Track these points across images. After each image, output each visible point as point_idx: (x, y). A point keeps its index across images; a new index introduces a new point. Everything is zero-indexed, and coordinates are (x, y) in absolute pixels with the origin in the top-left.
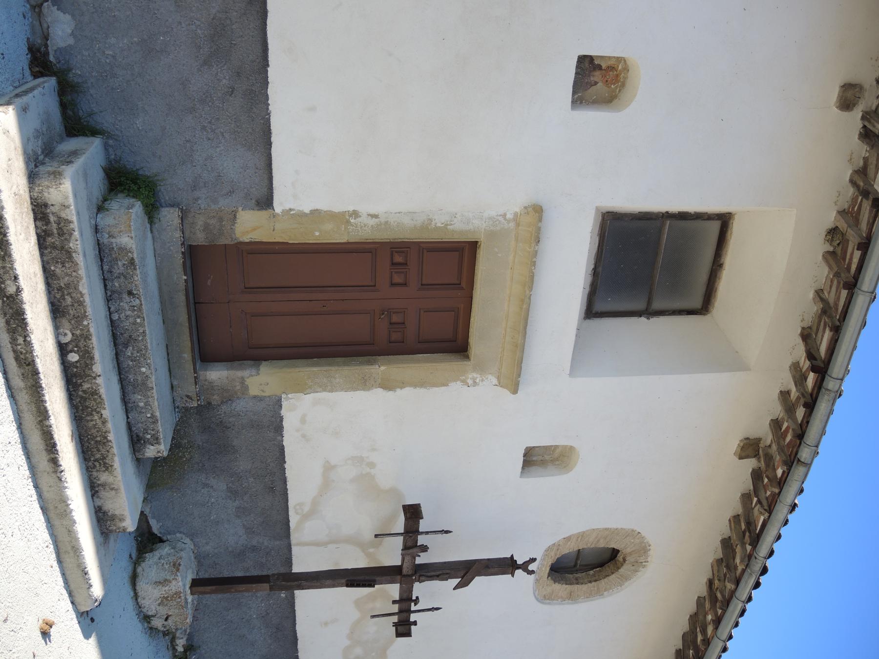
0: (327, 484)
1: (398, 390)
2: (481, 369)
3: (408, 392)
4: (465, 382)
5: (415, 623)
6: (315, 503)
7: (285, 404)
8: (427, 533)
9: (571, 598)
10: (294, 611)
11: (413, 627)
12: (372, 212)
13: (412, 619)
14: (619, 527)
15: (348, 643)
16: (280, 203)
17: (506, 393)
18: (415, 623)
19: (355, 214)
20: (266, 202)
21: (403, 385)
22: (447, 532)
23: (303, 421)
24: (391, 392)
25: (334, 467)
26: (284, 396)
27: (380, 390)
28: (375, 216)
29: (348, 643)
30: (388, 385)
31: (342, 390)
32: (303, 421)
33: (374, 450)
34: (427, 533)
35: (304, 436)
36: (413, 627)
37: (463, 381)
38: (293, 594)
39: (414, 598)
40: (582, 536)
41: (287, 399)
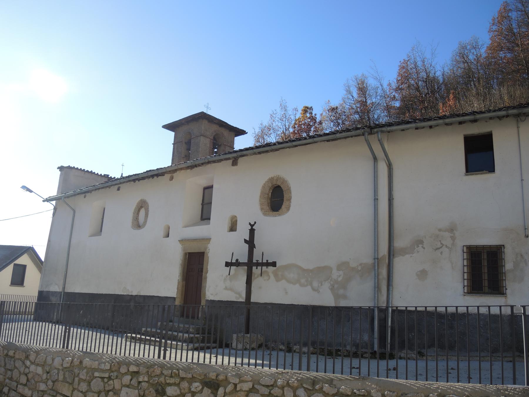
0: (231, 289)
1: (208, 269)
2: (206, 248)
3: (209, 267)
4: (208, 252)
5: (267, 261)
6: (236, 293)
7: (208, 299)
8: (232, 260)
9: (289, 200)
10: (278, 304)
11: (269, 262)
12: (178, 276)
13: (266, 262)
14: (260, 192)
15: (298, 285)
16: (175, 296)
17: (211, 240)
18: (267, 261)
19: (178, 280)
20: (174, 299)
21: (207, 268)
22: (233, 253)
23: (212, 294)
24: (208, 271)
25: (226, 287)
26: (206, 299)
27: (207, 274)
28: (179, 276)
29: (298, 285)
30: (207, 272)
31: (206, 284)
32: (212, 294)
33: (222, 276)
34: (232, 260)
35: (216, 295)
36: (269, 262)
37: (208, 253)
38: (252, 302)
39: (256, 262)
40: (262, 204)
41: (207, 298)
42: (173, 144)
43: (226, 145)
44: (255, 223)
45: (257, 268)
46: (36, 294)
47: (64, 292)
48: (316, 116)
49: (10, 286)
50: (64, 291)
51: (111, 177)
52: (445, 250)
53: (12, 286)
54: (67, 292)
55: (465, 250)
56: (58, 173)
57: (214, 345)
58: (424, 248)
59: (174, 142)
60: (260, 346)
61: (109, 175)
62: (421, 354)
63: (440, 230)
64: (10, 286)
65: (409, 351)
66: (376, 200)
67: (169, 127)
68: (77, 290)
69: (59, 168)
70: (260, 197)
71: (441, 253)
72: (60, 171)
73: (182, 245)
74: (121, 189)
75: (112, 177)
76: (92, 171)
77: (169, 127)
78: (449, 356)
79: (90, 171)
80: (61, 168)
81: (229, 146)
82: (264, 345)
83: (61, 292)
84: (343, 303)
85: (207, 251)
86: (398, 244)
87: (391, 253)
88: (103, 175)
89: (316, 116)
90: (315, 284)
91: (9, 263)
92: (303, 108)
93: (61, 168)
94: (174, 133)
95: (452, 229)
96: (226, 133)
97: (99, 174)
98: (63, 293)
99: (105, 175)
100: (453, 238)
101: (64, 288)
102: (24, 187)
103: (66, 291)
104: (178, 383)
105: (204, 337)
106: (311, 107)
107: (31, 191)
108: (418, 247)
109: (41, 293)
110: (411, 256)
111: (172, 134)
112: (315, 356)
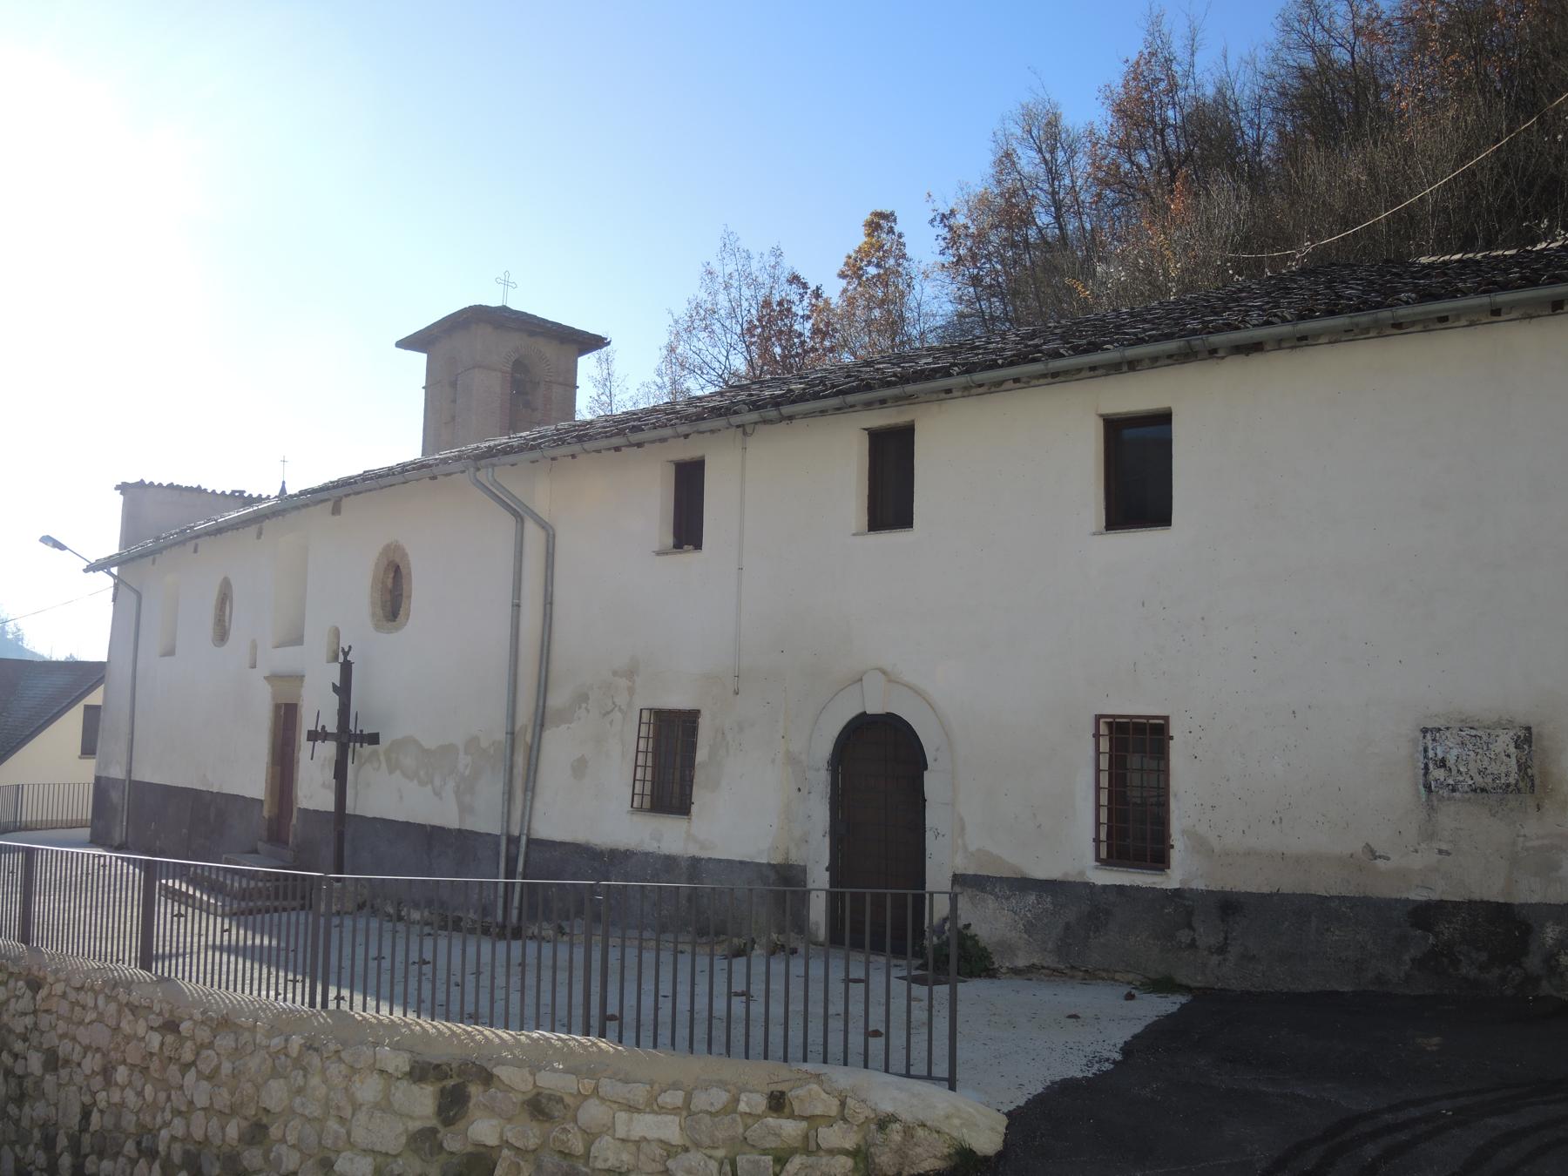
5: (361, 731)
9: (410, 597)
17: (306, 680)
18: (361, 731)
42: (423, 388)
43: (550, 382)
44: (350, 647)
45: (361, 746)
46: (92, 780)
47: (130, 780)
48: (901, 240)
49: (80, 758)
50: (130, 777)
51: (250, 495)
52: (617, 715)
53: (84, 758)
54: (137, 779)
55: (645, 717)
56: (118, 499)
57: (294, 904)
58: (588, 711)
59: (426, 382)
60: (361, 907)
61: (244, 492)
62: (561, 930)
63: (615, 673)
64: (80, 758)
65: (545, 923)
66: (517, 606)
67: (410, 343)
68: (147, 779)
69: (117, 488)
70: (372, 587)
71: (611, 723)
72: (121, 493)
73: (272, 686)
74: (199, 549)
75: (264, 497)
76: (199, 487)
77: (410, 343)
78: (630, 939)
79: (195, 486)
80: (123, 488)
81: (560, 384)
82: (368, 904)
83: (125, 780)
84: (468, 826)
85: (301, 702)
86: (556, 700)
87: (541, 721)
88: (228, 493)
89: (901, 240)
90: (437, 782)
91: (67, 706)
92: (867, 217)
93: (123, 488)
94: (424, 356)
95: (631, 673)
96: (549, 350)
97: (219, 492)
98: (127, 783)
99: (234, 492)
100: (631, 691)
101: (129, 772)
102: (48, 540)
103: (137, 777)
104: (846, 1116)
105: (277, 888)
106: (892, 214)
107: (62, 547)
108: (580, 708)
109: (98, 779)
110: (569, 728)
111: (421, 358)
112: (295, 912)
